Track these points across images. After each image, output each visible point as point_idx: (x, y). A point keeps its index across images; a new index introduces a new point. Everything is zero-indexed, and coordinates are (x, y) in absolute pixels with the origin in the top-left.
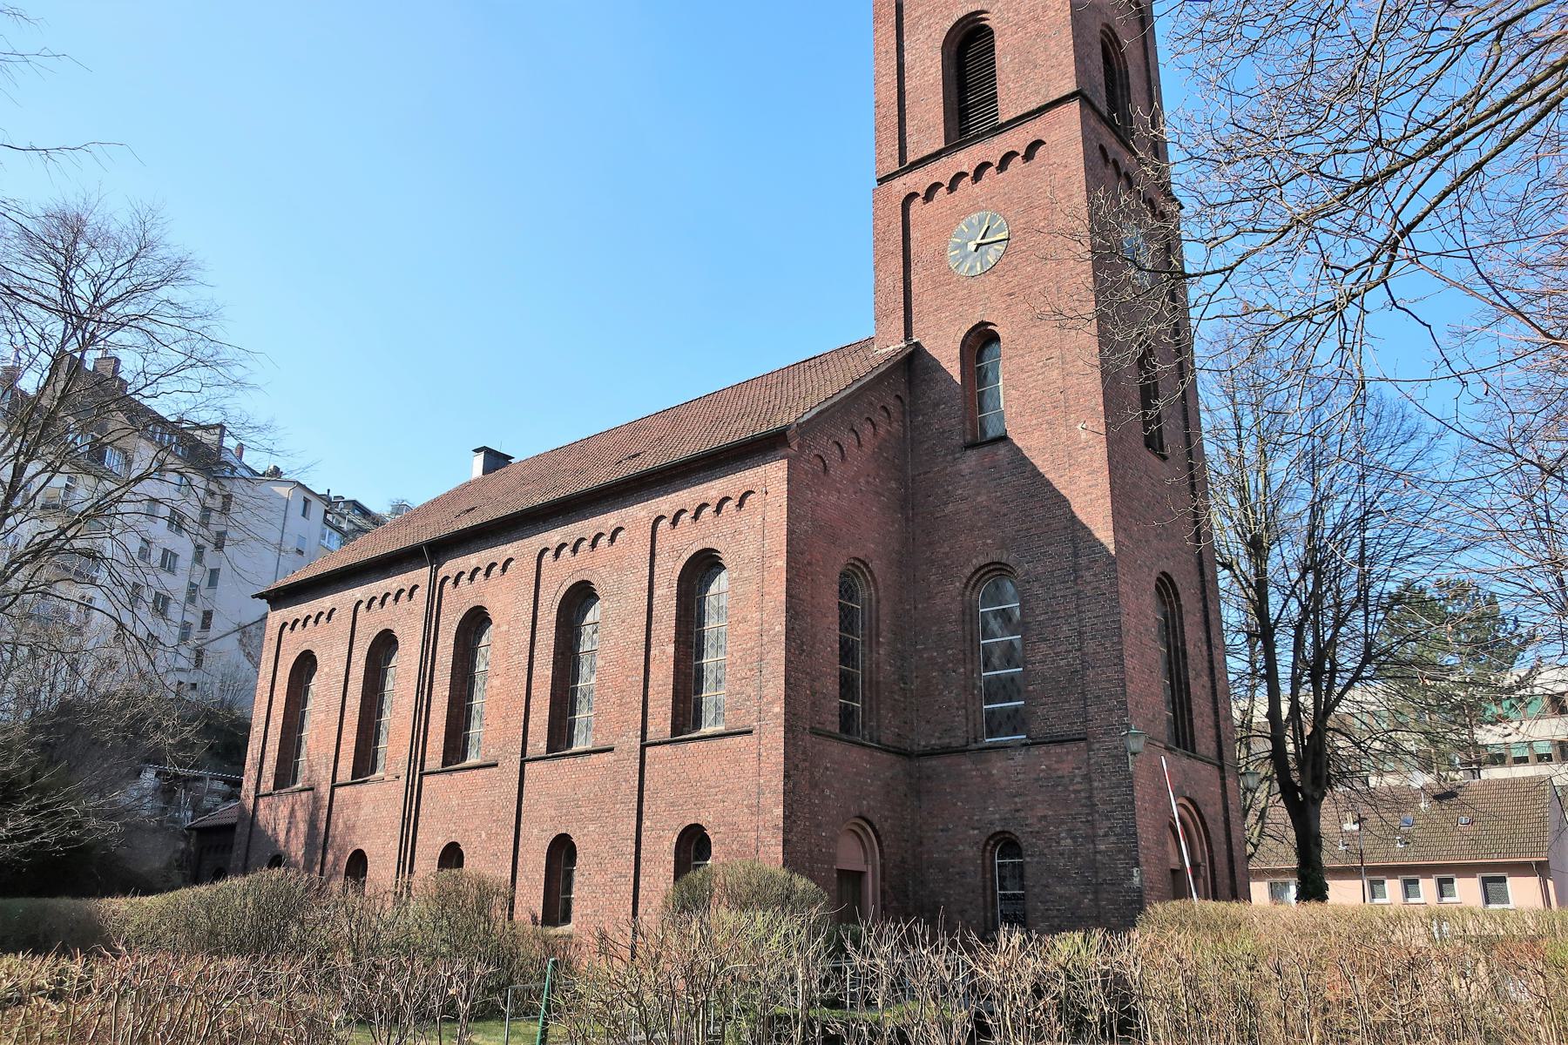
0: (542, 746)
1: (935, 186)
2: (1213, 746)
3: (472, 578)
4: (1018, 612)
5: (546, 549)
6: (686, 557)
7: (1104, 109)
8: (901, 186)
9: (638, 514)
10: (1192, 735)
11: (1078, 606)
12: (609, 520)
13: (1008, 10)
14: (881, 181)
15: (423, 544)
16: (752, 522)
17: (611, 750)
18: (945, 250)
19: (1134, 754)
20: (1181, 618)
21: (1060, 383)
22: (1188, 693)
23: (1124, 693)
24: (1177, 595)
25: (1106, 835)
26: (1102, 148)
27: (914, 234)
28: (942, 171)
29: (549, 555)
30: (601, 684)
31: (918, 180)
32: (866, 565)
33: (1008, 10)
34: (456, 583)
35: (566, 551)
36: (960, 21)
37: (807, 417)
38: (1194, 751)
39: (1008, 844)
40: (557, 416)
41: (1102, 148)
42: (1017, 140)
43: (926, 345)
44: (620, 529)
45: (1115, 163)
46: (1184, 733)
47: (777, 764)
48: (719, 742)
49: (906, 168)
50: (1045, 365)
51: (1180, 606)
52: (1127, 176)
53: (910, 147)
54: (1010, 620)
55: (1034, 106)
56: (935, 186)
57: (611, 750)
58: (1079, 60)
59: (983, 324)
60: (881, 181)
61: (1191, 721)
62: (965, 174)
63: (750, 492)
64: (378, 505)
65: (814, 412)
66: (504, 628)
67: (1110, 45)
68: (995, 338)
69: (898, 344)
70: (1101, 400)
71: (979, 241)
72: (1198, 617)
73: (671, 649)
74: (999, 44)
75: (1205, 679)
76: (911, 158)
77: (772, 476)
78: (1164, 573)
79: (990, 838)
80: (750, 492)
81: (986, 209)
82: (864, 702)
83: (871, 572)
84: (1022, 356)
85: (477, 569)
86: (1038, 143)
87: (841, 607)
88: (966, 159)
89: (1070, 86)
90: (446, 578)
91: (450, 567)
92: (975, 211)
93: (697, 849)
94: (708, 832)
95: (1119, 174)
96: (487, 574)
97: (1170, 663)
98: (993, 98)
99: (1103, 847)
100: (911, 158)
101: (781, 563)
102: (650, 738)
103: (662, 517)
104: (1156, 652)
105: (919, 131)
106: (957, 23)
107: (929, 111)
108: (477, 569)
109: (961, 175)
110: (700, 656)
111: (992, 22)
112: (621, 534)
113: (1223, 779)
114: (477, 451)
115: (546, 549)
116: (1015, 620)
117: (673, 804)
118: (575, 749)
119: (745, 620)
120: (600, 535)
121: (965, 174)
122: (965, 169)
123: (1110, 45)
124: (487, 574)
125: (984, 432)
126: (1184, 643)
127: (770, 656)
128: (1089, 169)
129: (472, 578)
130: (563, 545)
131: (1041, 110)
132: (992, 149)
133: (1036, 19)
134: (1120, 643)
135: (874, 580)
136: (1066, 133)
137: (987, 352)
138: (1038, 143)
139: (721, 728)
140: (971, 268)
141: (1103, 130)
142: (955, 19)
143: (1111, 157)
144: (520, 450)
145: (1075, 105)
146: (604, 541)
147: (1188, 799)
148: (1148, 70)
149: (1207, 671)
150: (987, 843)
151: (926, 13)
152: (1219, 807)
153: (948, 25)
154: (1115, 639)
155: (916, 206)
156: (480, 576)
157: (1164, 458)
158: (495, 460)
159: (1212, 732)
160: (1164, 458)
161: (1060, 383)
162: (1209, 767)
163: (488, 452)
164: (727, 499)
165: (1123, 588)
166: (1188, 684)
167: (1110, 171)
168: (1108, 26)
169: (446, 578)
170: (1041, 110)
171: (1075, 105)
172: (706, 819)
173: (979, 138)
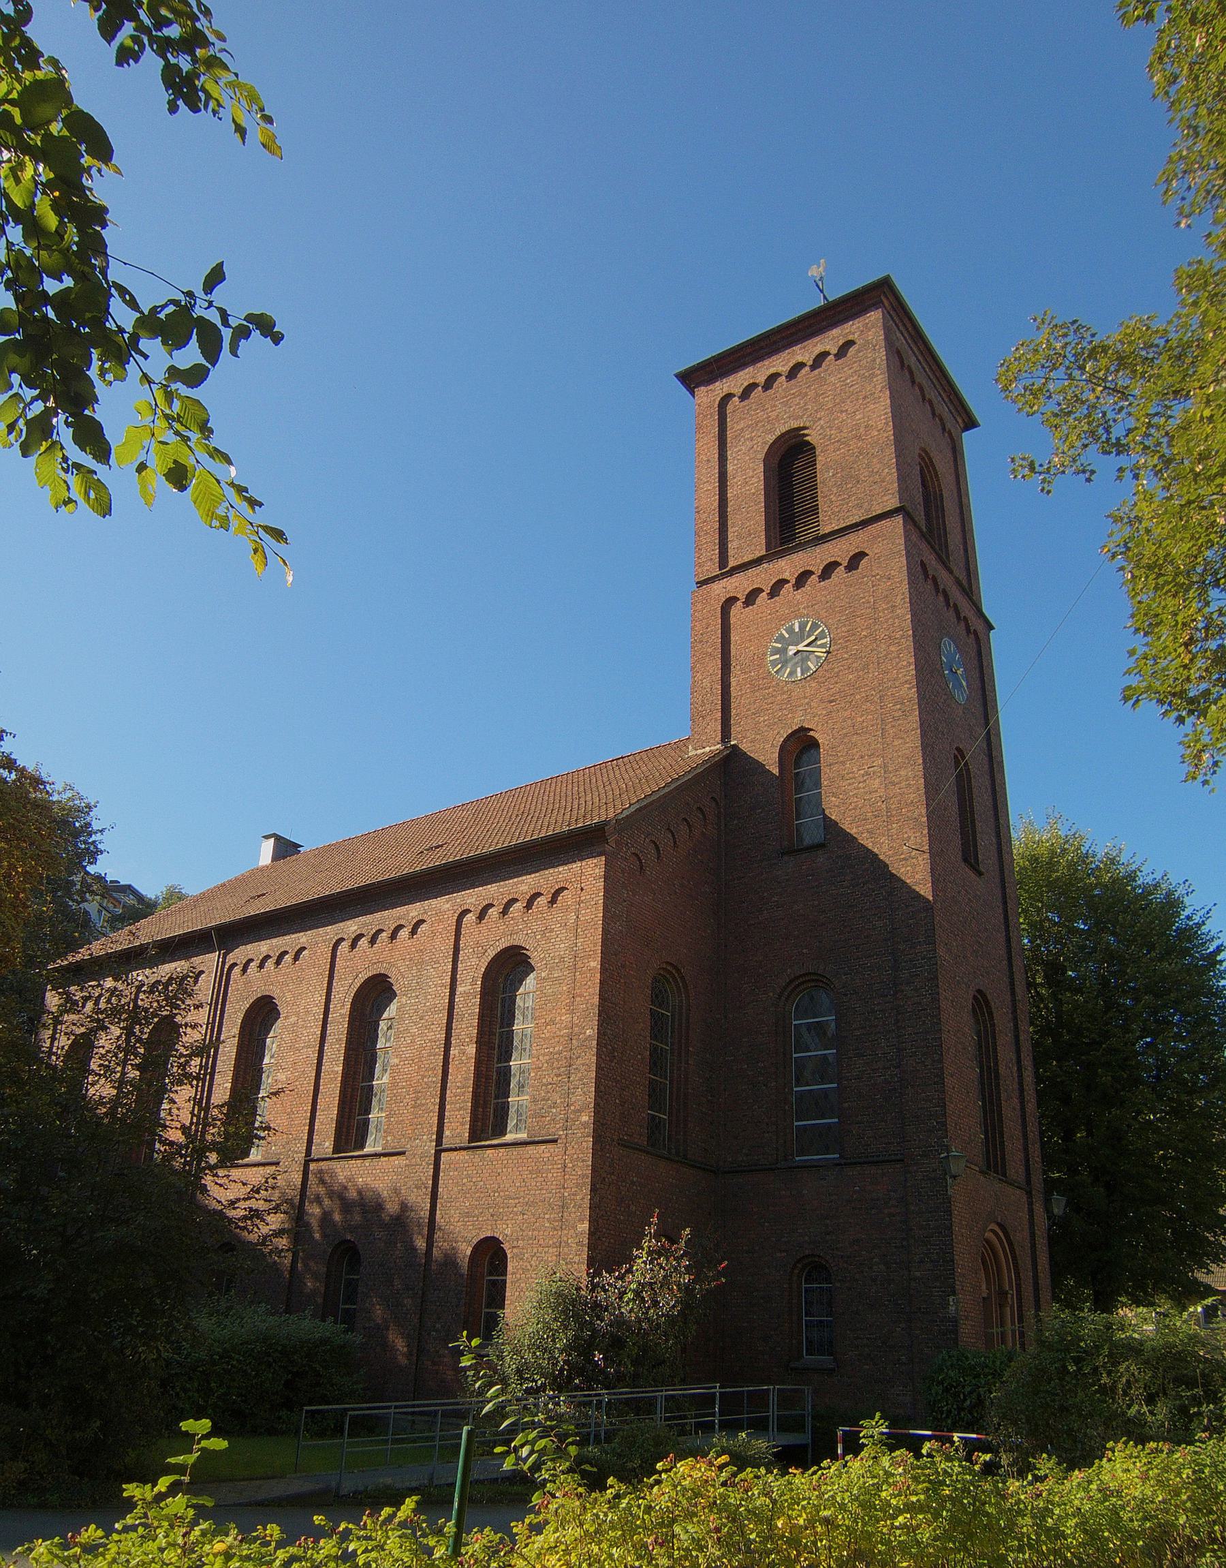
0: (328, 1145)
1: (756, 592)
2: (1022, 1170)
3: (261, 966)
4: (833, 1025)
5: (342, 939)
6: (492, 953)
7: (923, 525)
8: (722, 590)
9: (443, 906)
10: (1003, 1158)
11: (897, 1021)
12: (413, 911)
13: (831, 428)
14: (701, 584)
15: (212, 928)
16: (565, 926)
17: (403, 1153)
18: (764, 654)
19: (954, 1177)
20: (994, 1038)
21: (881, 792)
22: (1000, 1114)
23: (944, 1115)
24: (991, 1014)
25: (922, 1261)
26: (923, 564)
27: (734, 637)
28: (762, 577)
29: (345, 946)
30: (394, 1084)
31: (738, 585)
32: (678, 970)
33: (831, 428)
34: (244, 970)
35: (363, 942)
36: (783, 435)
37: (626, 813)
38: (1004, 1175)
39: (816, 1268)
40: (352, 808)
41: (923, 564)
42: (839, 550)
43: (744, 747)
44: (423, 921)
45: (934, 579)
46: (995, 1156)
47: (583, 1176)
48: (520, 1149)
49: (726, 570)
50: (867, 774)
51: (993, 1025)
52: (944, 591)
53: (732, 546)
54: (825, 1033)
55: (856, 519)
56: (756, 592)
57: (403, 1153)
58: (902, 478)
59: (803, 730)
60: (701, 584)
61: (1002, 1143)
62: (787, 582)
63: (563, 889)
64: (151, 889)
65: (633, 809)
66: (293, 1019)
67: (927, 469)
68: (814, 744)
69: (714, 747)
70: (924, 811)
71: (800, 647)
72: (1010, 1037)
73: (472, 1050)
74: (820, 459)
75: (1016, 1102)
76: (732, 563)
77: (587, 875)
78: (979, 991)
79: (799, 1261)
80: (563, 889)
81: (808, 616)
82: (670, 1114)
83: (682, 978)
84: (843, 763)
85: (268, 957)
86: (861, 555)
87: (652, 1012)
88: (787, 567)
89: (892, 502)
90: (235, 965)
91: (240, 954)
92: (796, 617)
93: (491, 1263)
94: (505, 1246)
95: (937, 591)
96: (278, 963)
97: (982, 1084)
98: (815, 510)
99: (918, 1274)
100: (732, 563)
101: (595, 964)
102: (446, 1143)
103: (467, 911)
104: (973, 1073)
105: (739, 537)
106: (779, 438)
107: (748, 519)
108: (268, 957)
109: (782, 582)
110: (509, 1059)
111: (813, 437)
112: (423, 927)
113: (1031, 1204)
114: (267, 837)
115: (342, 939)
116: (829, 1034)
117: (468, 1215)
118: (368, 1150)
119: (553, 1022)
120: (401, 927)
121: (787, 582)
122: (786, 576)
123: (927, 469)
124: (278, 963)
125: (800, 839)
126: (996, 1064)
127: (580, 1061)
128: (912, 583)
129: (261, 966)
130: (361, 936)
131: (864, 523)
132: (814, 558)
133: (859, 438)
134: (940, 1061)
135: (685, 986)
136: (889, 547)
137: (805, 758)
138: (861, 555)
139: (523, 1136)
140: (791, 674)
141: (924, 546)
142: (778, 433)
143: (931, 573)
144: (309, 842)
145: (899, 520)
146: (404, 934)
147: (1000, 1225)
148: (960, 496)
149: (1017, 1093)
150: (795, 1266)
151: (748, 426)
152: (1026, 1233)
153: (771, 438)
154: (936, 1057)
155: (736, 611)
156: (270, 964)
157: (980, 874)
158: (285, 849)
159: (1021, 1155)
160: (980, 874)
161: (881, 792)
162: (1018, 1192)
163: (278, 839)
164: (539, 894)
165: (943, 1004)
166: (999, 1106)
167: (929, 586)
168: (924, 450)
169: (235, 965)
170: (864, 523)
171: (899, 520)
172: (504, 1231)
173: (801, 546)
